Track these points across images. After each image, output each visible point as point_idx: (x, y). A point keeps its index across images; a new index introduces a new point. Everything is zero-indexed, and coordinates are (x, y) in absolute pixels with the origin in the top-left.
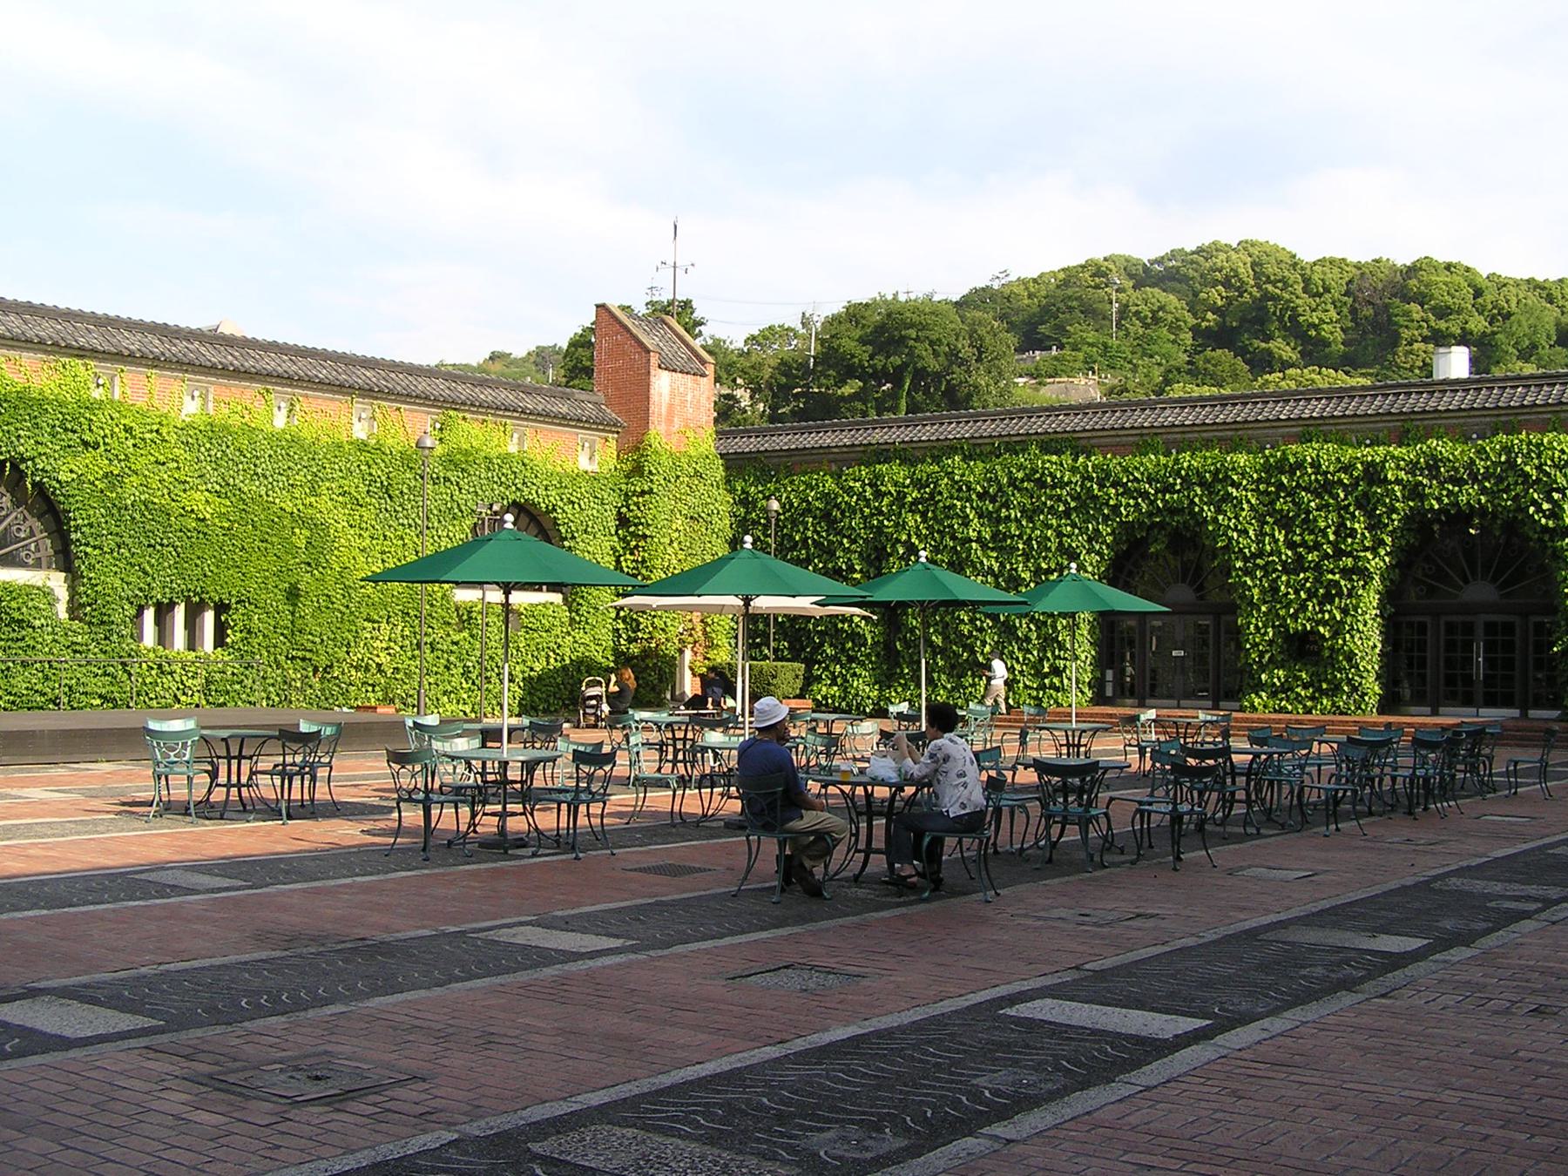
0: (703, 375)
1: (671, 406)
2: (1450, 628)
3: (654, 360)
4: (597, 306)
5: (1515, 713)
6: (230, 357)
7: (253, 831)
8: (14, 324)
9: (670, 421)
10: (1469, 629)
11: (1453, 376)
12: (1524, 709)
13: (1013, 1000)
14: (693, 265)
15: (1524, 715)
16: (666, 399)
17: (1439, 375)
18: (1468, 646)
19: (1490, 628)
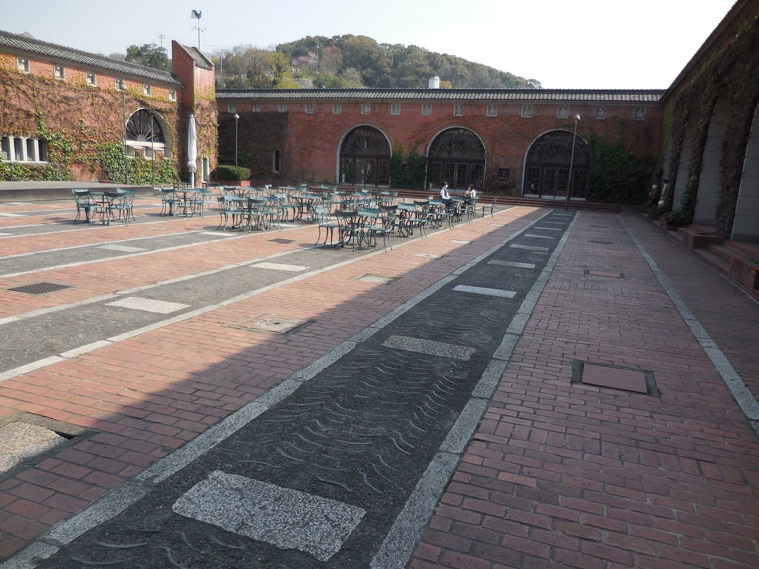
0: (211, 70)
1: (201, 80)
2: (448, 165)
3: (195, 63)
4: (172, 41)
5: (538, 196)
6: (35, 48)
7: (516, 209)
8: (4, 41)
9: (201, 85)
10: (453, 166)
11: (435, 88)
12: (541, 195)
13: (108, 301)
14: (206, 29)
15: (540, 197)
16: (199, 77)
17: (430, 87)
18: (453, 171)
19: (460, 166)
